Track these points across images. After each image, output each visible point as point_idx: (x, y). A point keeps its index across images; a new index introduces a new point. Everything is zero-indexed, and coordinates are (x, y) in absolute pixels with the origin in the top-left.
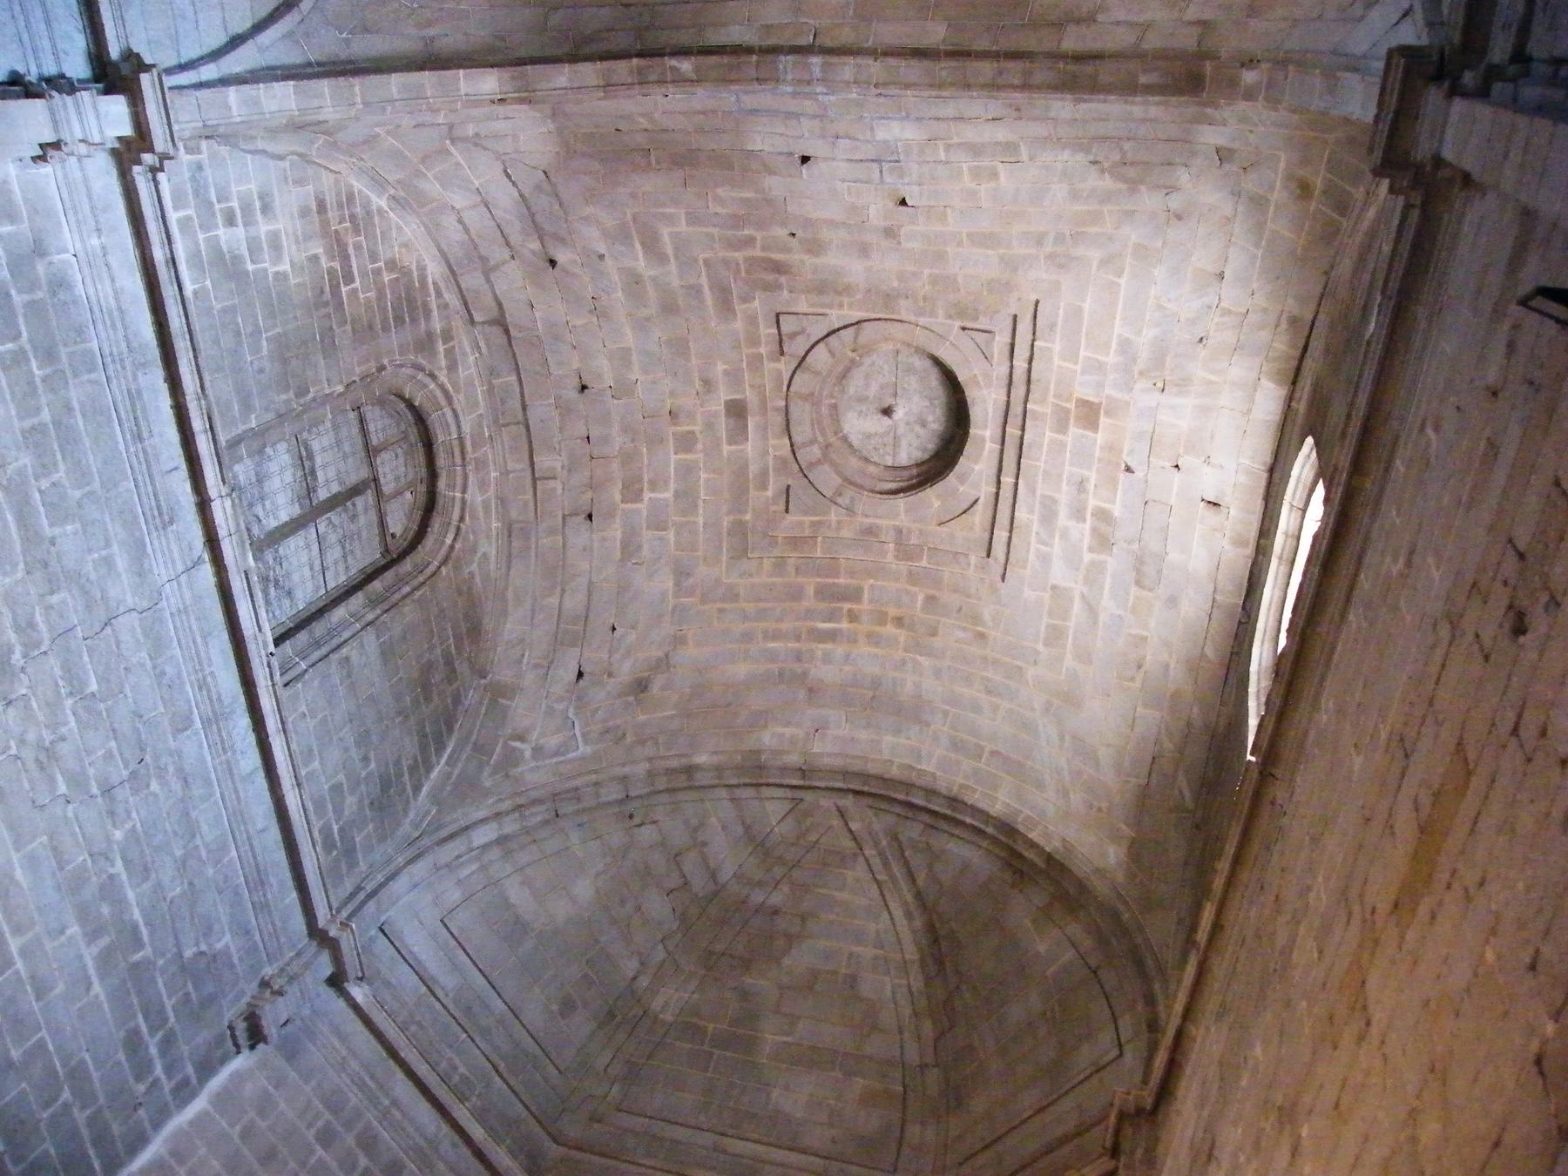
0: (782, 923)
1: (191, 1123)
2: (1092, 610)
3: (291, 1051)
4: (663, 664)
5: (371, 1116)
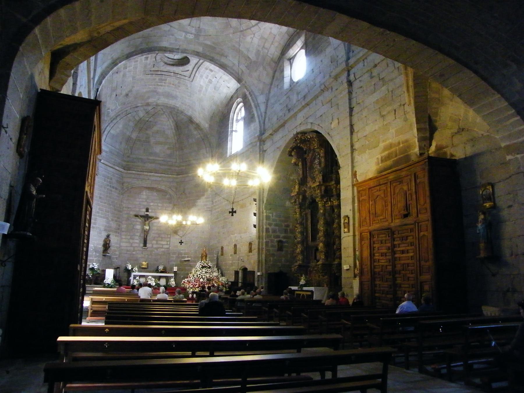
2: (206, 90)
4: (130, 91)
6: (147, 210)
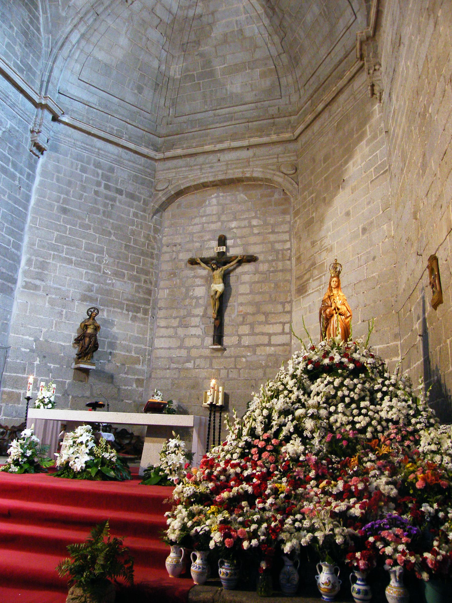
0: (204, 19)
1: (39, 185)
3: (55, 149)
5: (94, 157)
6: (222, 241)
